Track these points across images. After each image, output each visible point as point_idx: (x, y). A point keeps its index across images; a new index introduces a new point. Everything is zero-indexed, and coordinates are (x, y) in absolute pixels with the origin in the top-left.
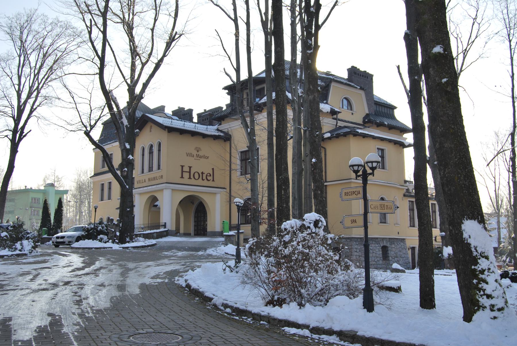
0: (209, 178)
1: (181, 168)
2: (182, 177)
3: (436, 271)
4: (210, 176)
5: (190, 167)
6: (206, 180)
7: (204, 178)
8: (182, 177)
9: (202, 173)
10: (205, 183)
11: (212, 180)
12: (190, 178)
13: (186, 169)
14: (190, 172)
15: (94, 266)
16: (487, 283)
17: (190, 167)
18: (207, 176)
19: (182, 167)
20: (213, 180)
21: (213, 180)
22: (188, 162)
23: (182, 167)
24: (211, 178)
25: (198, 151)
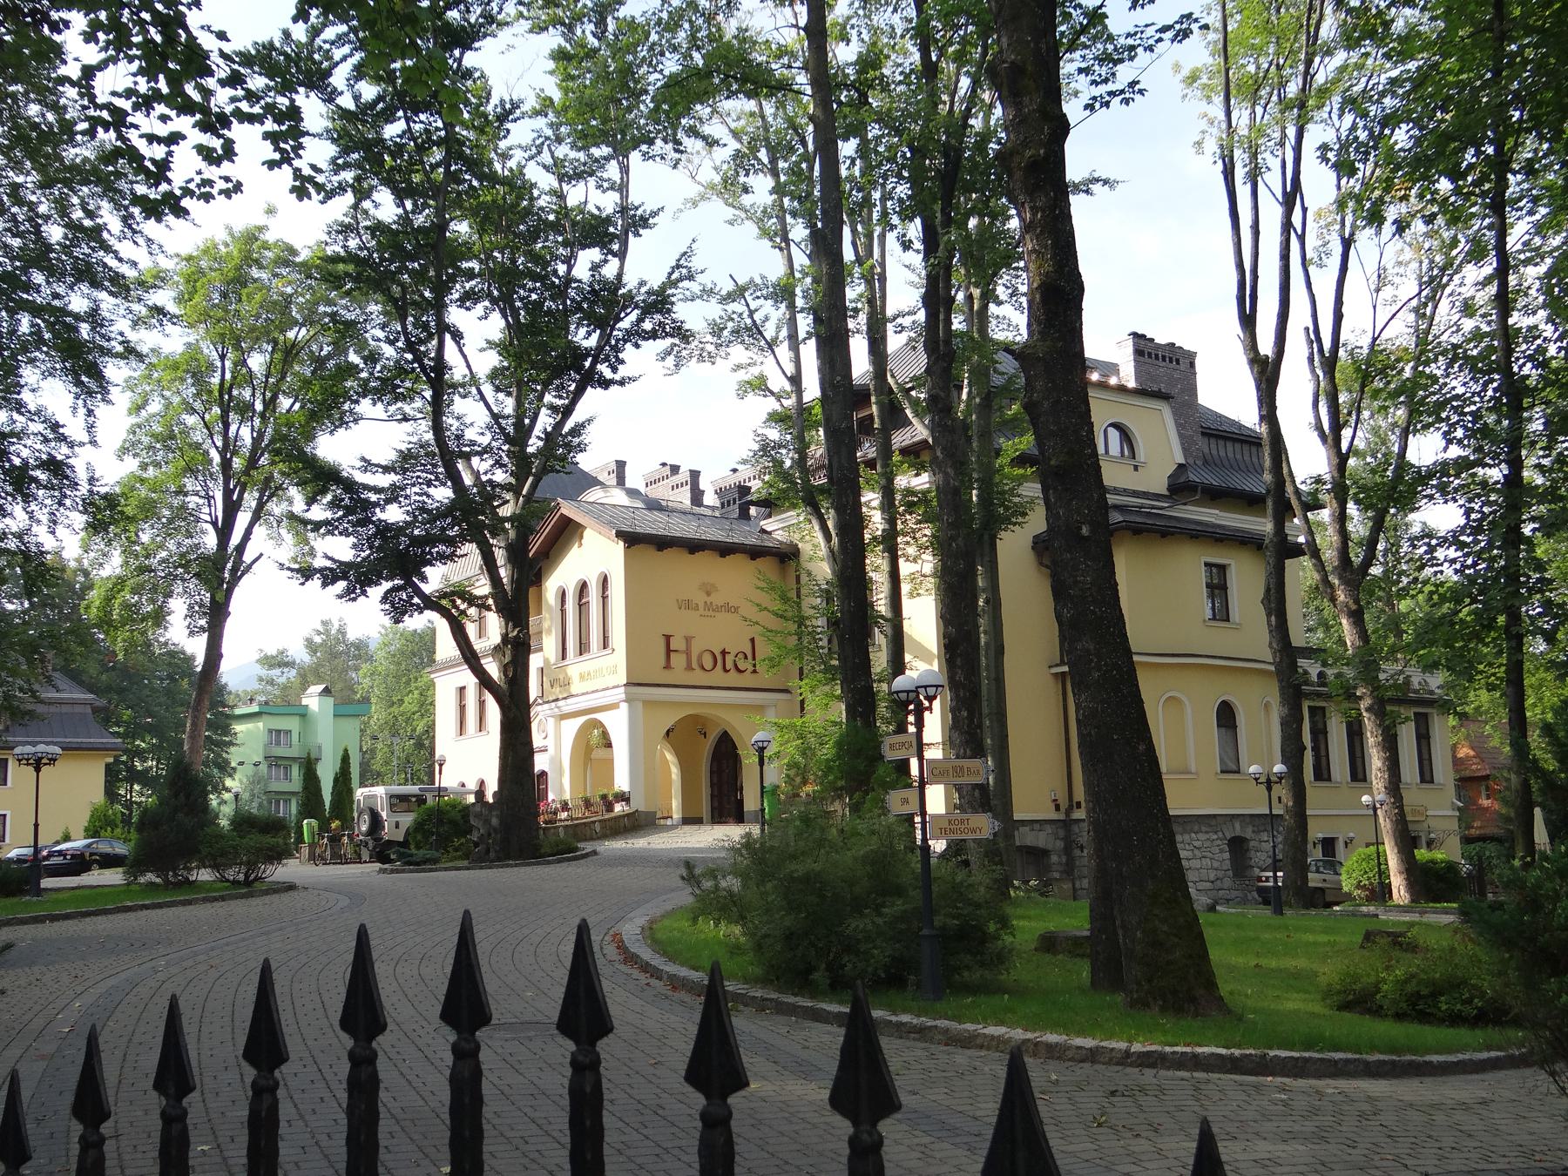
2: (668, 666)
3: (1087, 933)
7: (729, 665)
8: (668, 666)
9: (724, 653)
10: (733, 678)
11: (751, 668)
12: (689, 667)
14: (688, 653)
17: (688, 640)
19: (668, 638)
23: (668, 638)
25: (708, 594)
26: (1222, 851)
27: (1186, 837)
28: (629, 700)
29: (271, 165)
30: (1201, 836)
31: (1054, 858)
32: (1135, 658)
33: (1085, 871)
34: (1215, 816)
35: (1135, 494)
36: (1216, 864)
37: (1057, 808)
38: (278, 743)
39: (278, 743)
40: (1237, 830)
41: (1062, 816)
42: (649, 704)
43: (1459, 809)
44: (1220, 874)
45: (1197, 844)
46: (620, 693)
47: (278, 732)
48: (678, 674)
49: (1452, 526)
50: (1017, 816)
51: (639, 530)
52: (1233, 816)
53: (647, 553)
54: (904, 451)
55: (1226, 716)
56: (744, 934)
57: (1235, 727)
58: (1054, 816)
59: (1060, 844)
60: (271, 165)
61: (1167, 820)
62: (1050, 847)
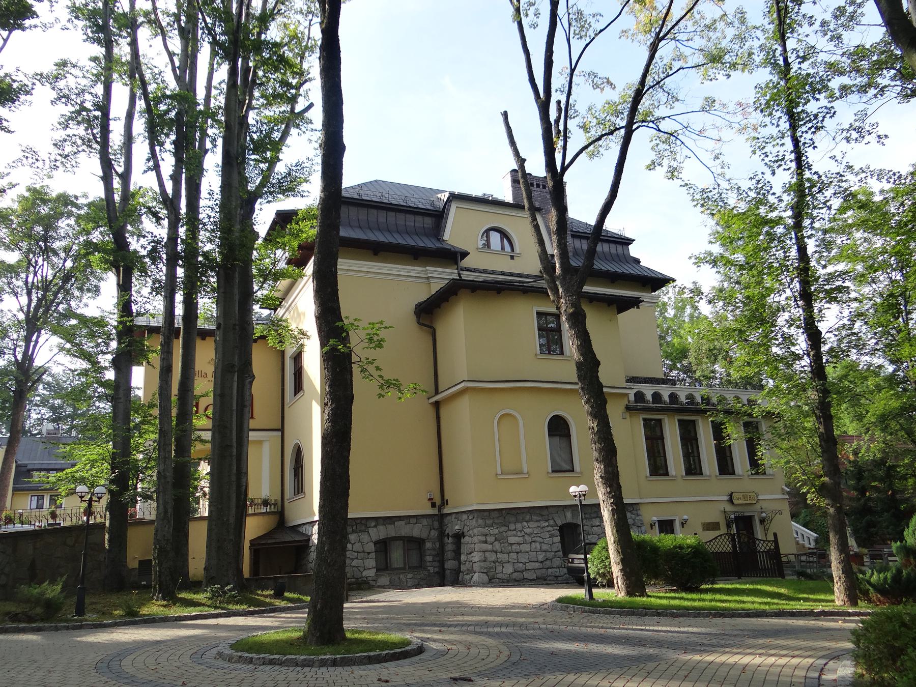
26: (552, 536)
27: (519, 526)
29: (695, 206)
30: (532, 525)
31: (428, 545)
32: (605, 390)
33: (428, 552)
34: (547, 507)
35: (503, 274)
36: (545, 547)
37: (433, 505)
40: (569, 517)
41: (435, 511)
43: (788, 493)
44: (550, 555)
45: (528, 531)
49: (16, 260)
50: (625, 501)
52: (565, 506)
55: (558, 428)
57: (568, 436)
58: (430, 511)
59: (434, 534)
60: (695, 206)
61: (346, 519)
62: (424, 536)
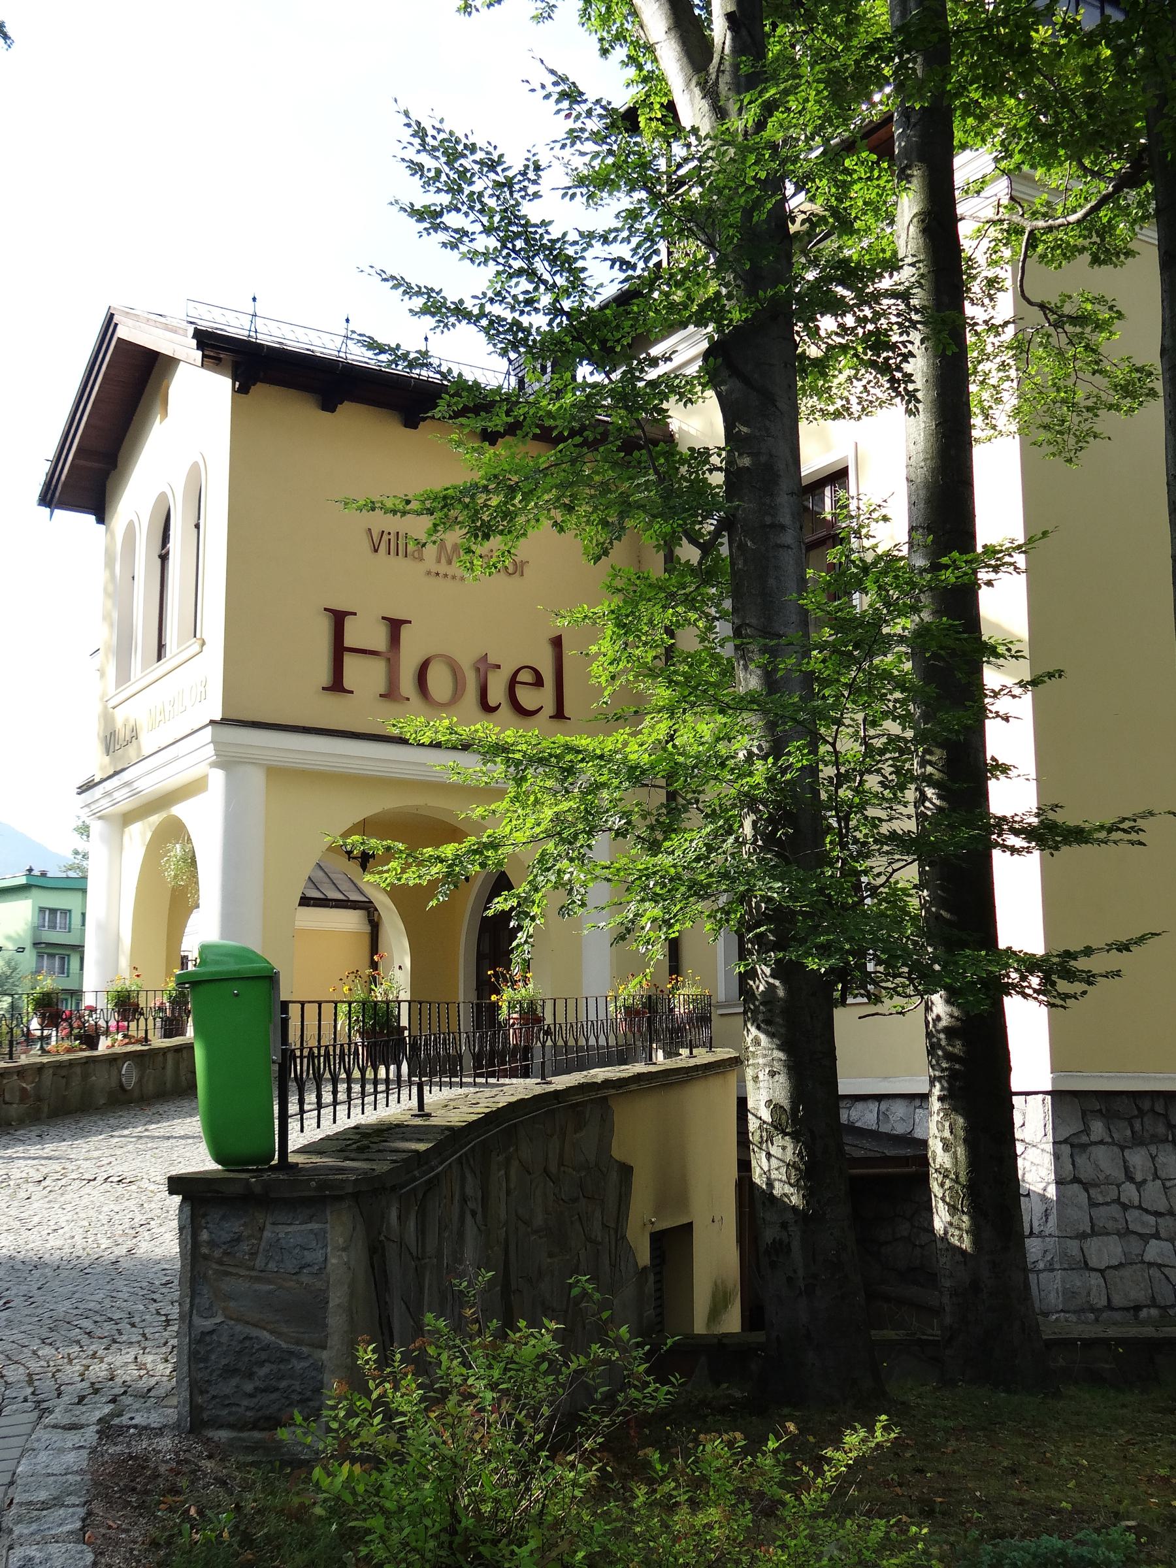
0: (527, 697)
1: (323, 629)
2: (337, 685)
4: (539, 682)
5: (395, 626)
6: (505, 711)
7: (497, 694)
8: (337, 685)
9: (484, 667)
11: (549, 708)
12: (391, 694)
13: (364, 632)
15: (181, 1038)
16: (444, 245)
17: (395, 626)
18: (513, 683)
19: (339, 618)
20: (559, 714)
21: (559, 714)
22: (376, 589)
23: (339, 618)
24: (543, 698)
28: (226, 761)
38: (53, 926)
39: (53, 926)
42: (278, 774)
46: (203, 746)
47: (53, 911)
48: (363, 703)
51: (264, 339)
53: (297, 415)
54: (431, 1536)
56: (881, 90)
